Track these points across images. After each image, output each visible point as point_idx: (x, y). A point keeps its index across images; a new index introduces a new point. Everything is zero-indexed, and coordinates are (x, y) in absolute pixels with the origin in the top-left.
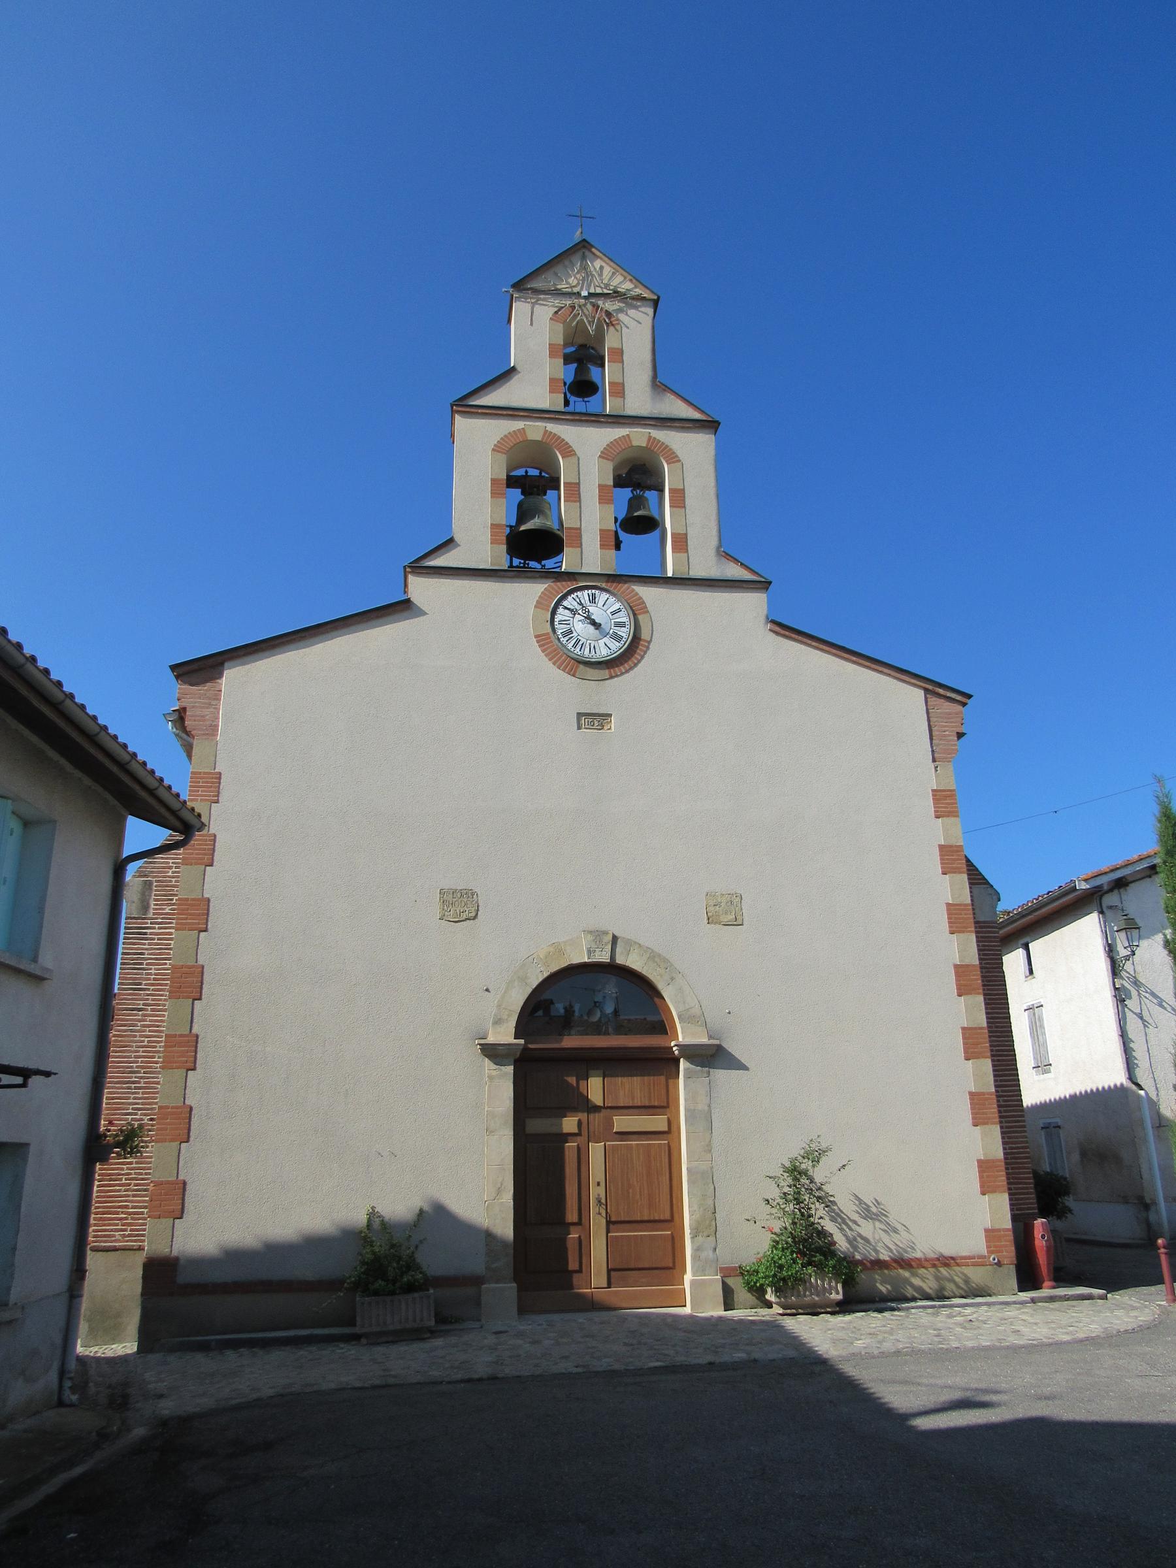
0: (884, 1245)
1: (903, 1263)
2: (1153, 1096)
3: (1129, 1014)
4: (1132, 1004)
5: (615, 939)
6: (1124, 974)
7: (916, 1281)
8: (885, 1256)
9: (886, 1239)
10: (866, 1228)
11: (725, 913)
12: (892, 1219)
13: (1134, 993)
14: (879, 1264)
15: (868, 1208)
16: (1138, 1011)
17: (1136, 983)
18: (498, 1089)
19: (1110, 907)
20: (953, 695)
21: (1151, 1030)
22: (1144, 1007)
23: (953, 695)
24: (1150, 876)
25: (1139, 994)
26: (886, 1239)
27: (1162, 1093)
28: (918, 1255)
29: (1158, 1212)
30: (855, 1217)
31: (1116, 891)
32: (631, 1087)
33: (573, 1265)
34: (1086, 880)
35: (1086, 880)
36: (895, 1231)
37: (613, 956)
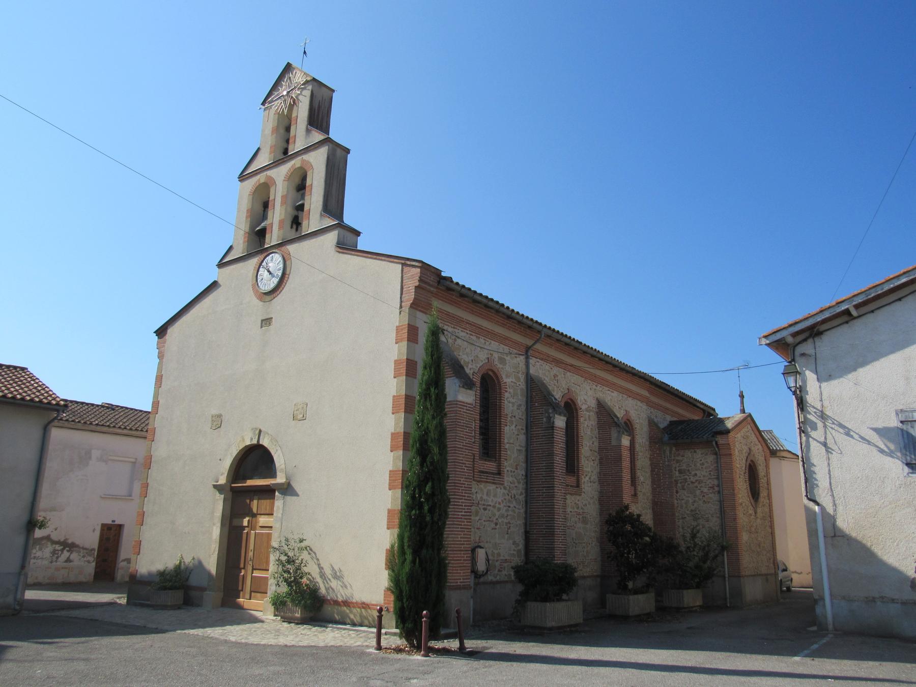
0: (341, 594)
1: (346, 603)
2: (830, 510)
3: (813, 444)
4: (817, 434)
5: (260, 431)
6: (811, 409)
7: (352, 616)
8: (340, 599)
9: (341, 590)
10: (334, 584)
11: (299, 416)
12: (345, 580)
13: (820, 425)
14: (336, 603)
15: (336, 573)
16: (822, 439)
17: (823, 416)
18: (217, 505)
19: (803, 355)
20: (414, 263)
21: (834, 457)
22: (829, 436)
23: (414, 263)
24: (847, 322)
25: (825, 426)
26: (341, 590)
27: (840, 508)
28: (354, 601)
29: (824, 606)
30: (330, 577)
31: (810, 341)
32: (265, 503)
33: (240, 588)
34: (765, 337)
35: (765, 337)
36: (346, 587)
37: (258, 441)
